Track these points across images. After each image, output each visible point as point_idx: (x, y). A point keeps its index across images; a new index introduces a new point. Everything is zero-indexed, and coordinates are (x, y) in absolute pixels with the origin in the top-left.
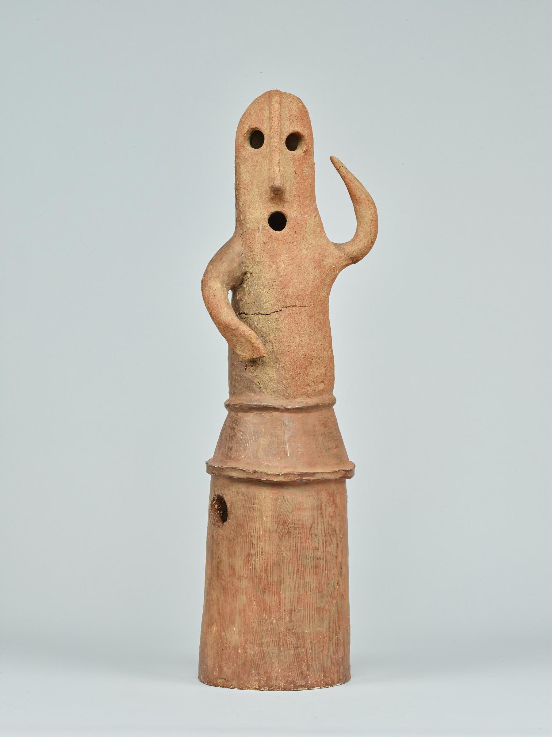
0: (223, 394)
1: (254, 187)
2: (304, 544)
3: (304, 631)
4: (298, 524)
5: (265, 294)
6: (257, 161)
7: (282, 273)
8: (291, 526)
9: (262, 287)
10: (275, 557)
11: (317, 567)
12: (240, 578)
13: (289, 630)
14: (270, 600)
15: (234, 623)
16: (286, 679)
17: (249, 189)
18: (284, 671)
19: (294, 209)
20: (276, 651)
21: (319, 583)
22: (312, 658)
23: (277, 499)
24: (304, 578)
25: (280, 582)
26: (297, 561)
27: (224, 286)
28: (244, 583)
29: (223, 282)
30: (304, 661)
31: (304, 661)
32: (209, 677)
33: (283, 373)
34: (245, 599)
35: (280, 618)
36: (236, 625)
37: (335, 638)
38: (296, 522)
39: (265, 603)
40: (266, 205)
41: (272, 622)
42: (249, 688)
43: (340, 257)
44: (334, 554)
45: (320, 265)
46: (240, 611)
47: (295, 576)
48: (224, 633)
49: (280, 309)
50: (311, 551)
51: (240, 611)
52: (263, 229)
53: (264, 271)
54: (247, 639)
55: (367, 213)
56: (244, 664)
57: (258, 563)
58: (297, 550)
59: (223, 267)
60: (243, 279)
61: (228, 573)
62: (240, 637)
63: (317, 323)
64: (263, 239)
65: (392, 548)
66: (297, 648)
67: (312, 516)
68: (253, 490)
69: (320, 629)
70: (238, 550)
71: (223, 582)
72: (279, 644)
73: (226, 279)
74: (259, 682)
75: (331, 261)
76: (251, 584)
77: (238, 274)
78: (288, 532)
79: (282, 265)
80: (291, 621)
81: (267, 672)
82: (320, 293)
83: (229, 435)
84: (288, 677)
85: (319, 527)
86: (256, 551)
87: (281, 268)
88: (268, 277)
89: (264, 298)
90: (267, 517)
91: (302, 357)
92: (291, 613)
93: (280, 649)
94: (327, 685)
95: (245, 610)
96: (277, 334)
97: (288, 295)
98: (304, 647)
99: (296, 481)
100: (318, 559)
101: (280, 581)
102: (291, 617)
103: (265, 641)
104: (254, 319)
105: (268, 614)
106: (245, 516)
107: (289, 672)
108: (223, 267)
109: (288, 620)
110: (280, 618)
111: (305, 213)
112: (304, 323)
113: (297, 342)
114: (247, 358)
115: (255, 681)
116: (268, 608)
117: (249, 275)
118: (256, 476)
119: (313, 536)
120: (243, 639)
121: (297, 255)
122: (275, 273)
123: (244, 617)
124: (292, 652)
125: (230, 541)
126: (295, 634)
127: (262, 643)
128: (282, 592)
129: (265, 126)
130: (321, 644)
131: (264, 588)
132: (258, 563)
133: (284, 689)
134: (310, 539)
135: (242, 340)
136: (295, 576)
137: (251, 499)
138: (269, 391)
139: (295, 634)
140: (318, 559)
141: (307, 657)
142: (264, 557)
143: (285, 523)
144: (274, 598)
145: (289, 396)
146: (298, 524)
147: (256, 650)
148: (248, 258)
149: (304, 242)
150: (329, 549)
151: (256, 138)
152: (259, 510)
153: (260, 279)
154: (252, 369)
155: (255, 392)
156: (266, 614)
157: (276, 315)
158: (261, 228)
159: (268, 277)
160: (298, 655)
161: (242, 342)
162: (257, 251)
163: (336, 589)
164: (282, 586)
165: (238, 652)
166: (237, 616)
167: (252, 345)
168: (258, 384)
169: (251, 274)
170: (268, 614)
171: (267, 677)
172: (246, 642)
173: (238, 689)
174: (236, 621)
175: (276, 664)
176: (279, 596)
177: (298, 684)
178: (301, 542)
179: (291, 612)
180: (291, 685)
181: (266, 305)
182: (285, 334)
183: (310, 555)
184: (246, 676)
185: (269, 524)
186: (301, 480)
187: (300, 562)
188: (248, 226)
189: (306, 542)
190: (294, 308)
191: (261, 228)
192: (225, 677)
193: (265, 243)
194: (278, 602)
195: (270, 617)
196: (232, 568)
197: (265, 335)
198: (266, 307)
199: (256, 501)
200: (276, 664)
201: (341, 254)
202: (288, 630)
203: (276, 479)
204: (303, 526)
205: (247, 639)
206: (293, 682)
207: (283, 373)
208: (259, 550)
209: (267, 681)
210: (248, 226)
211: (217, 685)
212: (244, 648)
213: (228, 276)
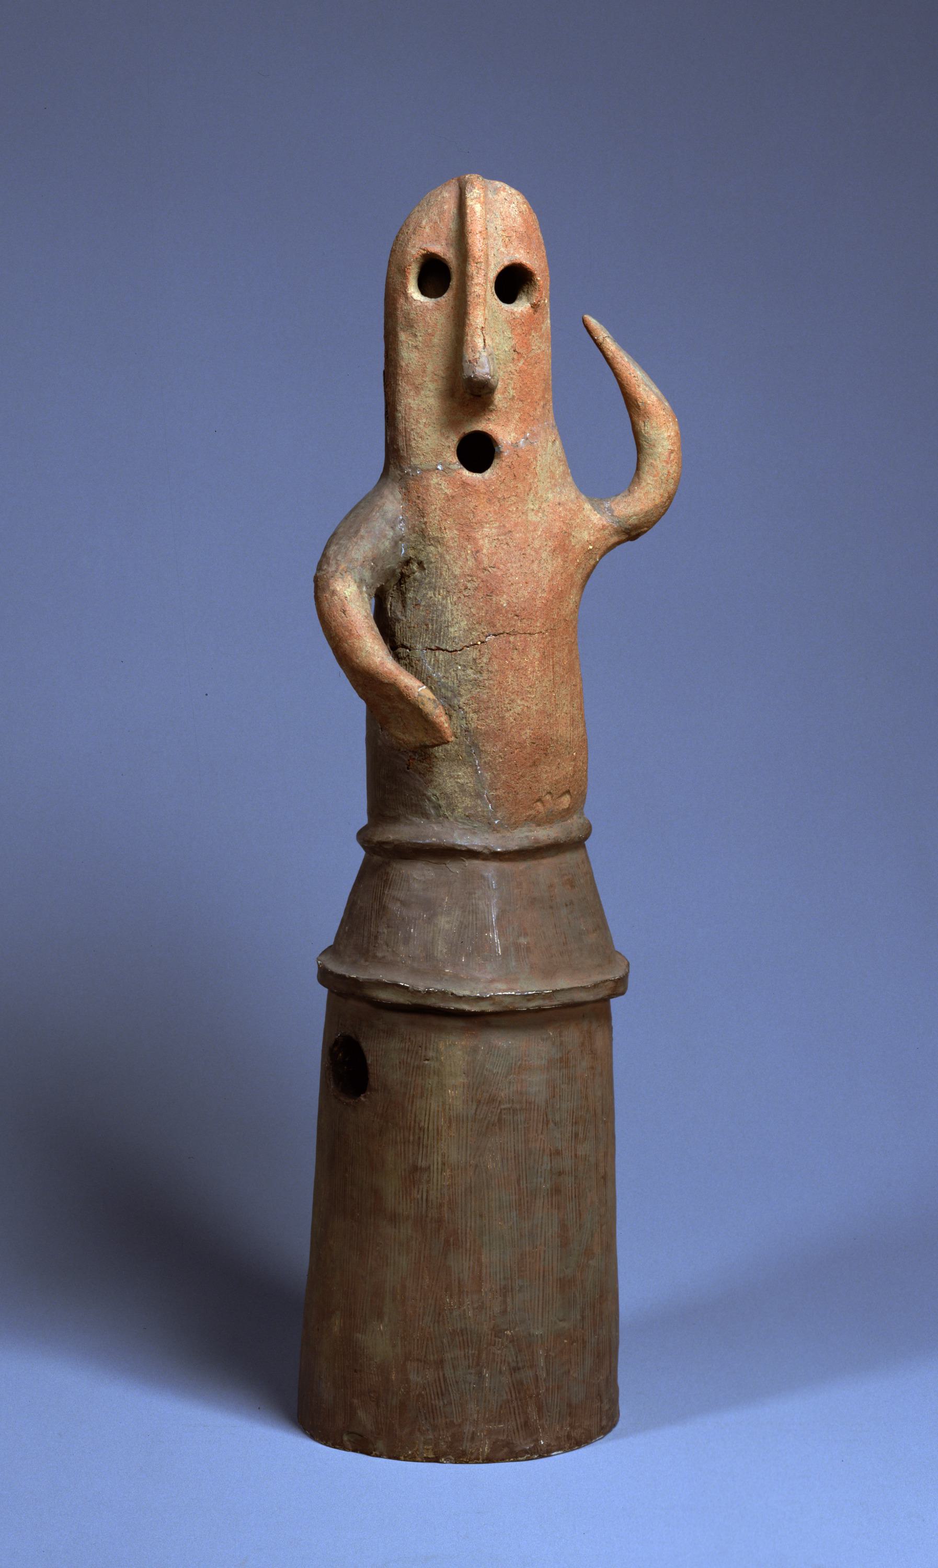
7: (486, 562)
22: (547, 1389)
23: (475, 1050)
30: (531, 1397)
33: (488, 775)
36: (386, 1319)
42: (413, 1459)
43: (604, 528)
50: (546, 1159)
53: (448, 557)
62: (394, 1346)
66: (516, 1369)
72: (478, 1365)
74: (436, 1445)
77: (393, 564)
78: (500, 1120)
79: (486, 546)
81: (452, 1422)
87: (485, 551)
90: (454, 1087)
92: (505, 1296)
96: (475, 692)
98: (531, 1367)
103: (448, 1356)
107: (500, 1423)
119: (551, 1125)
122: (471, 563)
133: (489, 1460)
141: (537, 1387)
142: (448, 1173)
155: (425, 815)
156: (451, 1297)
171: (453, 1436)
176: (479, 1260)
179: (505, 1291)
181: (452, 630)
190: (512, 638)
195: (461, 1304)
206: (508, 1444)
207: (488, 775)
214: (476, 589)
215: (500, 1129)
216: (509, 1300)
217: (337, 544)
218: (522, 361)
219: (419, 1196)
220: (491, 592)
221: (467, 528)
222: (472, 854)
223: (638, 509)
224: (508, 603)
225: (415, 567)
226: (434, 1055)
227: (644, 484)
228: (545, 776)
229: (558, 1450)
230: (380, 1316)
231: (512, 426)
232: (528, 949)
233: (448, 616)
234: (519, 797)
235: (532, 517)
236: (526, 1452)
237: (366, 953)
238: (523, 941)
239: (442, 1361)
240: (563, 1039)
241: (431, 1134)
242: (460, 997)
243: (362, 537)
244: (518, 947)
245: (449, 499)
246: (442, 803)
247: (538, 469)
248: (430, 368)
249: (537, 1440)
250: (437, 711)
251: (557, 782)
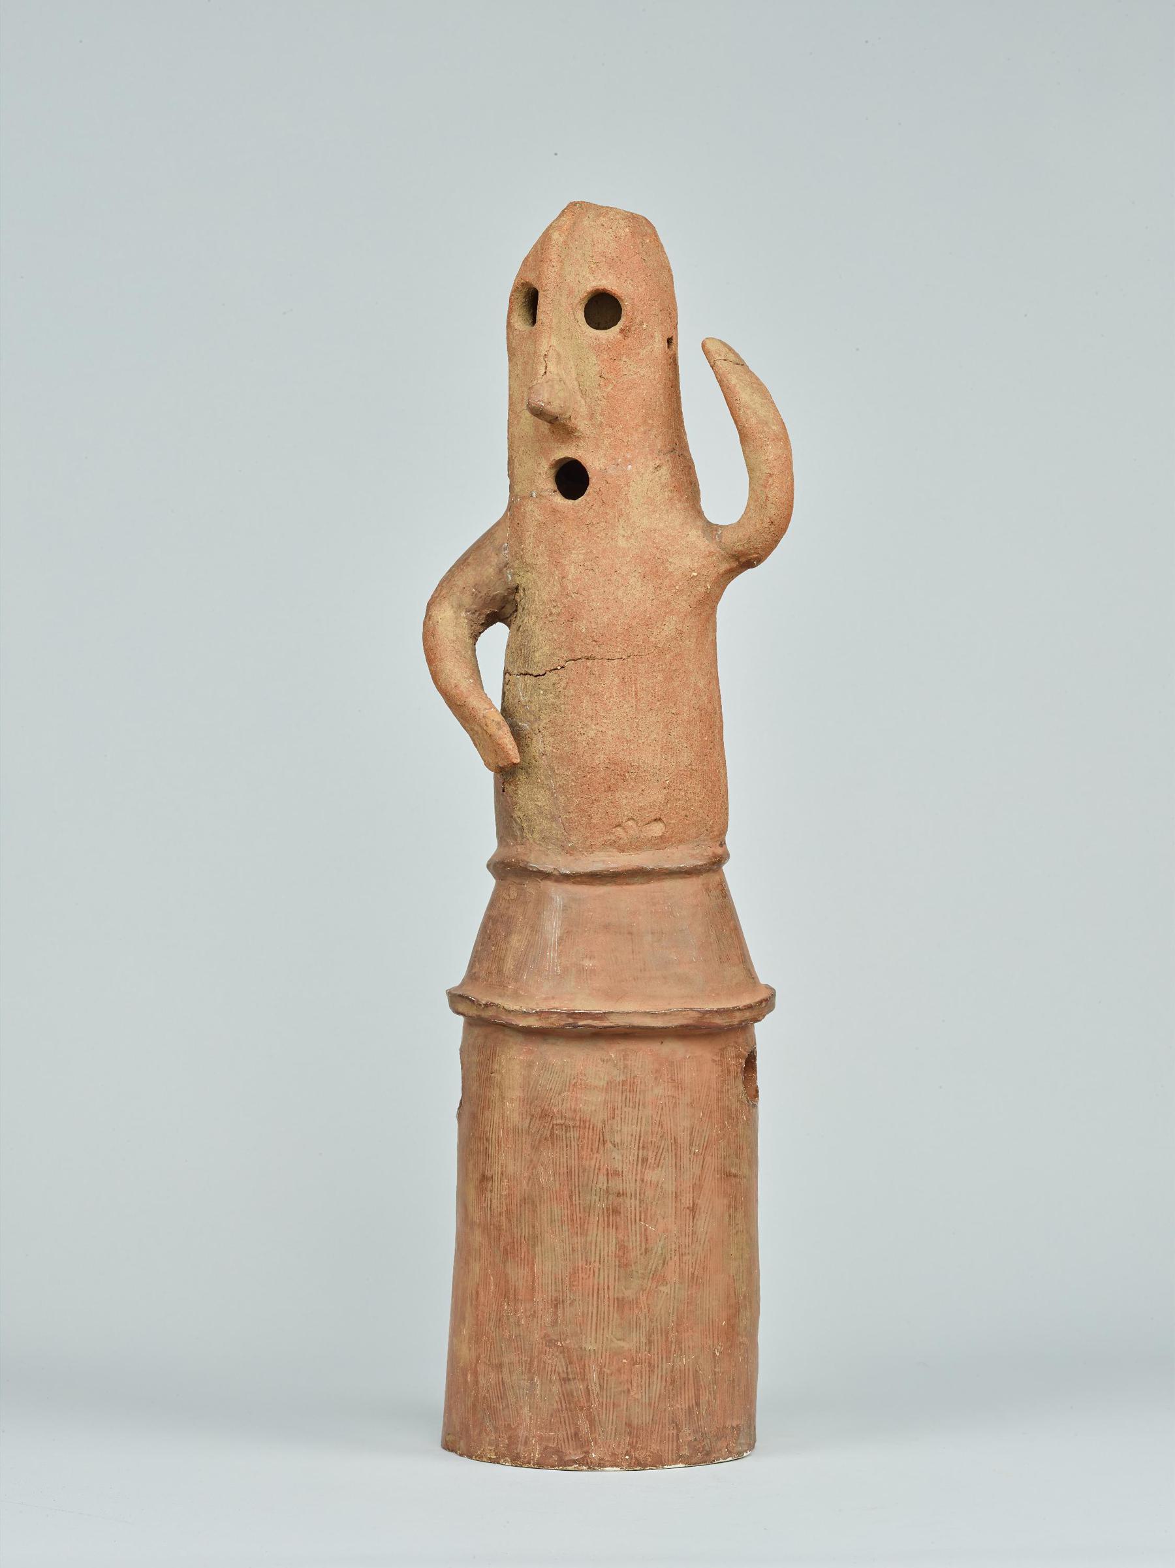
2: (586, 1163)
3: (584, 1345)
4: (574, 1119)
5: (538, 632)
7: (570, 587)
8: (559, 1122)
9: (534, 618)
11: (616, 1212)
13: (550, 1341)
16: (544, 1443)
18: (541, 1429)
19: (602, 452)
20: (527, 1384)
21: (622, 1247)
22: (600, 1404)
23: (530, 1065)
24: (584, 1233)
25: (534, 1239)
26: (571, 1197)
27: (463, 614)
29: (460, 606)
30: (582, 1409)
31: (582, 1409)
32: (461, 1440)
33: (562, 799)
35: (534, 1315)
37: (667, 1366)
38: (569, 1114)
43: (711, 554)
44: (670, 1188)
47: (565, 1228)
49: (562, 664)
50: (602, 1178)
52: (539, 496)
58: (569, 1173)
59: (470, 576)
63: (641, 694)
66: (566, 1380)
67: (606, 1102)
69: (621, 1343)
73: (467, 600)
75: (687, 562)
77: (500, 591)
78: (552, 1134)
79: (572, 571)
80: (554, 1323)
82: (656, 631)
84: (549, 1439)
85: (625, 1129)
87: (570, 577)
89: (535, 642)
92: (556, 1306)
93: (532, 1380)
94: (641, 1465)
95: (477, 1293)
98: (583, 1380)
99: (563, 1028)
100: (619, 1195)
101: (535, 1237)
102: (555, 1313)
103: (506, 1360)
104: (520, 686)
105: (512, 1304)
107: (551, 1430)
108: (470, 576)
109: (548, 1320)
111: (628, 461)
112: (608, 695)
115: (490, 1444)
116: (512, 1291)
117: (521, 592)
119: (609, 1145)
121: (604, 551)
124: (556, 1389)
126: (563, 1350)
130: (624, 1377)
133: (540, 1465)
134: (601, 1151)
136: (565, 1228)
138: (537, 836)
139: (563, 1350)
140: (619, 1195)
141: (588, 1400)
142: (505, 1183)
143: (545, 1115)
146: (574, 1119)
149: (622, 523)
150: (651, 1175)
152: (500, 1086)
160: (568, 1396)
162: (529, 541)
163: (671, 1263)
164: (538, 1249)
170: (512, 1304)
171: (510, 1437)
176: (532, 1270)
178: (580, 1158)
179: (556, 1303)
180: (553, 1459)
181: (537, 654)
182: (611, 722)
183: (600, 1185)
185: (516, 1115)
186: (575, 1027)
187: (575, 1199)
189: (591, 1159)
190: (589, 663)
194: (530, 1279)
195: (516, 1311)
197: (532, 718)
204: (584, 1124)
206: (557, 1452)
208: (497, 1169)
209: (509, 1445)
212: (475, 1373)
213: (474, 595)
214: (559, 614)
215: (553, 1144)
216: (560, 1312)
218: (611, 387)
220: (572, 618)
221: (556, 554)
222: (546, 876)
224: (587, 629)
228: (625, 802)
229: (612, 1466)
231: (602, 452)
232: (593, 971)
233: (535, 641)
234: (594, 821)
235: (622, 543)
236: (575, 1462)
237: (499, 981)
239: (501, 1365)
240: (629, 1063)
242: (510, 1011)
243: (469, 564)
245: (542, 525)
246: (525, 825)
247: (630, 495)
250: (500, 732)
251: (641, 809)
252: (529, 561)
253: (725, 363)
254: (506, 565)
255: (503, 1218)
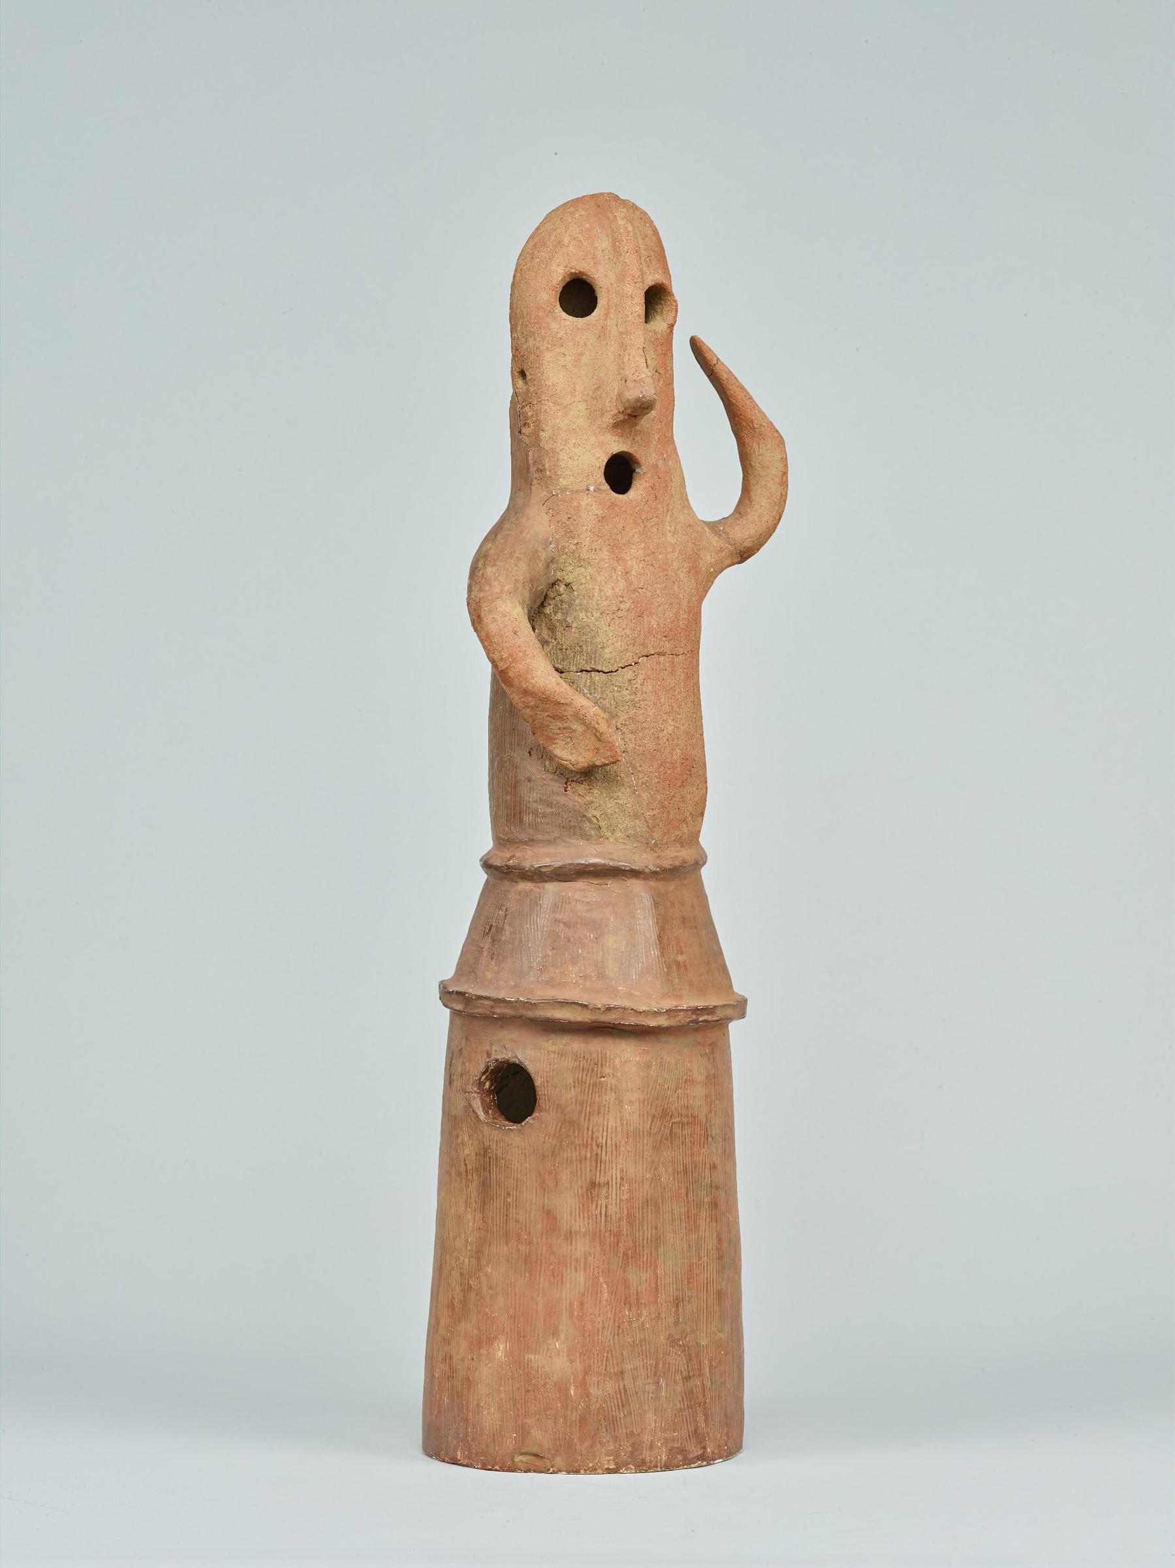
0: (481, 839)
1: (577, 399)
6: (585, 344)
7: (635, 581)
8: (677, 1119)
10: (647, 1187)
12: (570, 1236)
14: (638, 1279)
15: (555, 1334)
17: (565, 403)
20: (652, 1388)
24: (697, 1229)
25: (658, 1240)
28: (581, 1247)
33: (645, 796)
34: (582, 1280)
35: (658, 1317)
36: (562, 1336)
38: (684, 1112)
39: (627, 1287)
40: (602, 438)
41: (642, 1328)
42: (593, 1471)
43: (722, 550)
45: (694, 569)
46: (571, 1305)
48: (531, 1356)
51: (571, 1305)
52: (597, 490)
53: (599, 579)
54: (590, 1366)
55: (763, 453)
56: (583, 1419)
57: (613, 1202)
58: (685, 1171)
60: (546, 597)
61: (539, 1226)
62: (572, 1362)
64: (596, 510)
65: (833, 1159)
66: (687, 1378)
68: (597, 1046)
70: (565, 1176)
71: (522, 1248)
72: (655, 1374)
74: (617, 1455)
76: (598, 1246)
77: (542, 587)
79: (636, 568)
80: (677, 1323)
81: (632, 1432)
83: (489, 932)
84: (674, 1440)
86: (608, 1177)
87: (634, 573)
88: (609, 593)
90: (631, 1103)
91: (679, 761)
95: (582, 1303)
96: (632, 712)
97: (650, 631)
98: (700, 1376)
101: (658, 1238)
103: (628, 1367)
106: (582, 1104)
109: (671, 1320)
110: (658, 1317)
113: (670, 729)
114: (581, 765)
117: (562, 588)
118: (614, 1016)
120: (579, 1366)
122: (622, 584)
123: (581, 1318)
124: (679, 1388)
125: (544, 1156)
127: (622, 1373)
128: (660, 1261)
129: (601, 269)
131: (625, 1254)
132: (613, 1202)
133: (667, 1467)
135: (574, 727)
137: (593, 1069)
138: (618, 834)
141: (704, 1395)
142: (626, 1187)
143: (665, 1114)
144: (647, 1275)
145: (656, 845)
147: (610, 1386)
148: (562, 551)
151: (579, 296)
152: (615, 1089)
153: (591, 597)
154: (582, 789)
155: (587, 838)
156: (630, 1309)
157: (628, 674)
158: (592, 488)
159: (609, 593)
160: (689, 1394)
161: (574, 731)
162: (586, 538)
164: (661, 1250)
165: (567, 1395)
166: (565, 1316)
167: (599, 737)
168: (594, 820)
169: (567, 585)
172: (586, 1372)
173: (569, 1472)
174: (561, 1327)
175: (650, 1416)
177: (691, 1456)
181: (607, 651)
184: (586, 1444)
187: (690, 1195)
188: (563, 482)
190: (662, 659)
191: (592, 488)
192: (535, 1450)
193: (602, 520)
195: (639, 1315)
196: (549, 1215)
198: (608, 656)
199: (607, 1070)
200: (650, 1416)
201: (722, 544)
202: (673, 1342)
203: (653, 1023)
204: (694, 1120)
205: (590, 1366)
207: (645, 796)
208: (615, 1173)
209: (632, 1452)
210: (563, 482)
211: (512, 1469)
212: (583, 1385)
217: (494, 565)
219: (598, 1212)
222: (538, 876)
223: (752, 531)
225: (562, 588)
226: (611, 1071)
227: (757, 506)
230: (555, 1334)
238: (680, 958)
241: (609, 1150)
244: (678, 964)
246: (602, 824)
248: (579, 388)
249: (704, 1448)
252: (584, 555)
253: (696, 346)
254: (553, 560)
255: (624, 1223)
